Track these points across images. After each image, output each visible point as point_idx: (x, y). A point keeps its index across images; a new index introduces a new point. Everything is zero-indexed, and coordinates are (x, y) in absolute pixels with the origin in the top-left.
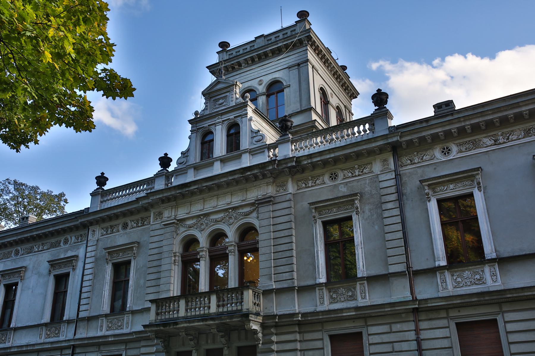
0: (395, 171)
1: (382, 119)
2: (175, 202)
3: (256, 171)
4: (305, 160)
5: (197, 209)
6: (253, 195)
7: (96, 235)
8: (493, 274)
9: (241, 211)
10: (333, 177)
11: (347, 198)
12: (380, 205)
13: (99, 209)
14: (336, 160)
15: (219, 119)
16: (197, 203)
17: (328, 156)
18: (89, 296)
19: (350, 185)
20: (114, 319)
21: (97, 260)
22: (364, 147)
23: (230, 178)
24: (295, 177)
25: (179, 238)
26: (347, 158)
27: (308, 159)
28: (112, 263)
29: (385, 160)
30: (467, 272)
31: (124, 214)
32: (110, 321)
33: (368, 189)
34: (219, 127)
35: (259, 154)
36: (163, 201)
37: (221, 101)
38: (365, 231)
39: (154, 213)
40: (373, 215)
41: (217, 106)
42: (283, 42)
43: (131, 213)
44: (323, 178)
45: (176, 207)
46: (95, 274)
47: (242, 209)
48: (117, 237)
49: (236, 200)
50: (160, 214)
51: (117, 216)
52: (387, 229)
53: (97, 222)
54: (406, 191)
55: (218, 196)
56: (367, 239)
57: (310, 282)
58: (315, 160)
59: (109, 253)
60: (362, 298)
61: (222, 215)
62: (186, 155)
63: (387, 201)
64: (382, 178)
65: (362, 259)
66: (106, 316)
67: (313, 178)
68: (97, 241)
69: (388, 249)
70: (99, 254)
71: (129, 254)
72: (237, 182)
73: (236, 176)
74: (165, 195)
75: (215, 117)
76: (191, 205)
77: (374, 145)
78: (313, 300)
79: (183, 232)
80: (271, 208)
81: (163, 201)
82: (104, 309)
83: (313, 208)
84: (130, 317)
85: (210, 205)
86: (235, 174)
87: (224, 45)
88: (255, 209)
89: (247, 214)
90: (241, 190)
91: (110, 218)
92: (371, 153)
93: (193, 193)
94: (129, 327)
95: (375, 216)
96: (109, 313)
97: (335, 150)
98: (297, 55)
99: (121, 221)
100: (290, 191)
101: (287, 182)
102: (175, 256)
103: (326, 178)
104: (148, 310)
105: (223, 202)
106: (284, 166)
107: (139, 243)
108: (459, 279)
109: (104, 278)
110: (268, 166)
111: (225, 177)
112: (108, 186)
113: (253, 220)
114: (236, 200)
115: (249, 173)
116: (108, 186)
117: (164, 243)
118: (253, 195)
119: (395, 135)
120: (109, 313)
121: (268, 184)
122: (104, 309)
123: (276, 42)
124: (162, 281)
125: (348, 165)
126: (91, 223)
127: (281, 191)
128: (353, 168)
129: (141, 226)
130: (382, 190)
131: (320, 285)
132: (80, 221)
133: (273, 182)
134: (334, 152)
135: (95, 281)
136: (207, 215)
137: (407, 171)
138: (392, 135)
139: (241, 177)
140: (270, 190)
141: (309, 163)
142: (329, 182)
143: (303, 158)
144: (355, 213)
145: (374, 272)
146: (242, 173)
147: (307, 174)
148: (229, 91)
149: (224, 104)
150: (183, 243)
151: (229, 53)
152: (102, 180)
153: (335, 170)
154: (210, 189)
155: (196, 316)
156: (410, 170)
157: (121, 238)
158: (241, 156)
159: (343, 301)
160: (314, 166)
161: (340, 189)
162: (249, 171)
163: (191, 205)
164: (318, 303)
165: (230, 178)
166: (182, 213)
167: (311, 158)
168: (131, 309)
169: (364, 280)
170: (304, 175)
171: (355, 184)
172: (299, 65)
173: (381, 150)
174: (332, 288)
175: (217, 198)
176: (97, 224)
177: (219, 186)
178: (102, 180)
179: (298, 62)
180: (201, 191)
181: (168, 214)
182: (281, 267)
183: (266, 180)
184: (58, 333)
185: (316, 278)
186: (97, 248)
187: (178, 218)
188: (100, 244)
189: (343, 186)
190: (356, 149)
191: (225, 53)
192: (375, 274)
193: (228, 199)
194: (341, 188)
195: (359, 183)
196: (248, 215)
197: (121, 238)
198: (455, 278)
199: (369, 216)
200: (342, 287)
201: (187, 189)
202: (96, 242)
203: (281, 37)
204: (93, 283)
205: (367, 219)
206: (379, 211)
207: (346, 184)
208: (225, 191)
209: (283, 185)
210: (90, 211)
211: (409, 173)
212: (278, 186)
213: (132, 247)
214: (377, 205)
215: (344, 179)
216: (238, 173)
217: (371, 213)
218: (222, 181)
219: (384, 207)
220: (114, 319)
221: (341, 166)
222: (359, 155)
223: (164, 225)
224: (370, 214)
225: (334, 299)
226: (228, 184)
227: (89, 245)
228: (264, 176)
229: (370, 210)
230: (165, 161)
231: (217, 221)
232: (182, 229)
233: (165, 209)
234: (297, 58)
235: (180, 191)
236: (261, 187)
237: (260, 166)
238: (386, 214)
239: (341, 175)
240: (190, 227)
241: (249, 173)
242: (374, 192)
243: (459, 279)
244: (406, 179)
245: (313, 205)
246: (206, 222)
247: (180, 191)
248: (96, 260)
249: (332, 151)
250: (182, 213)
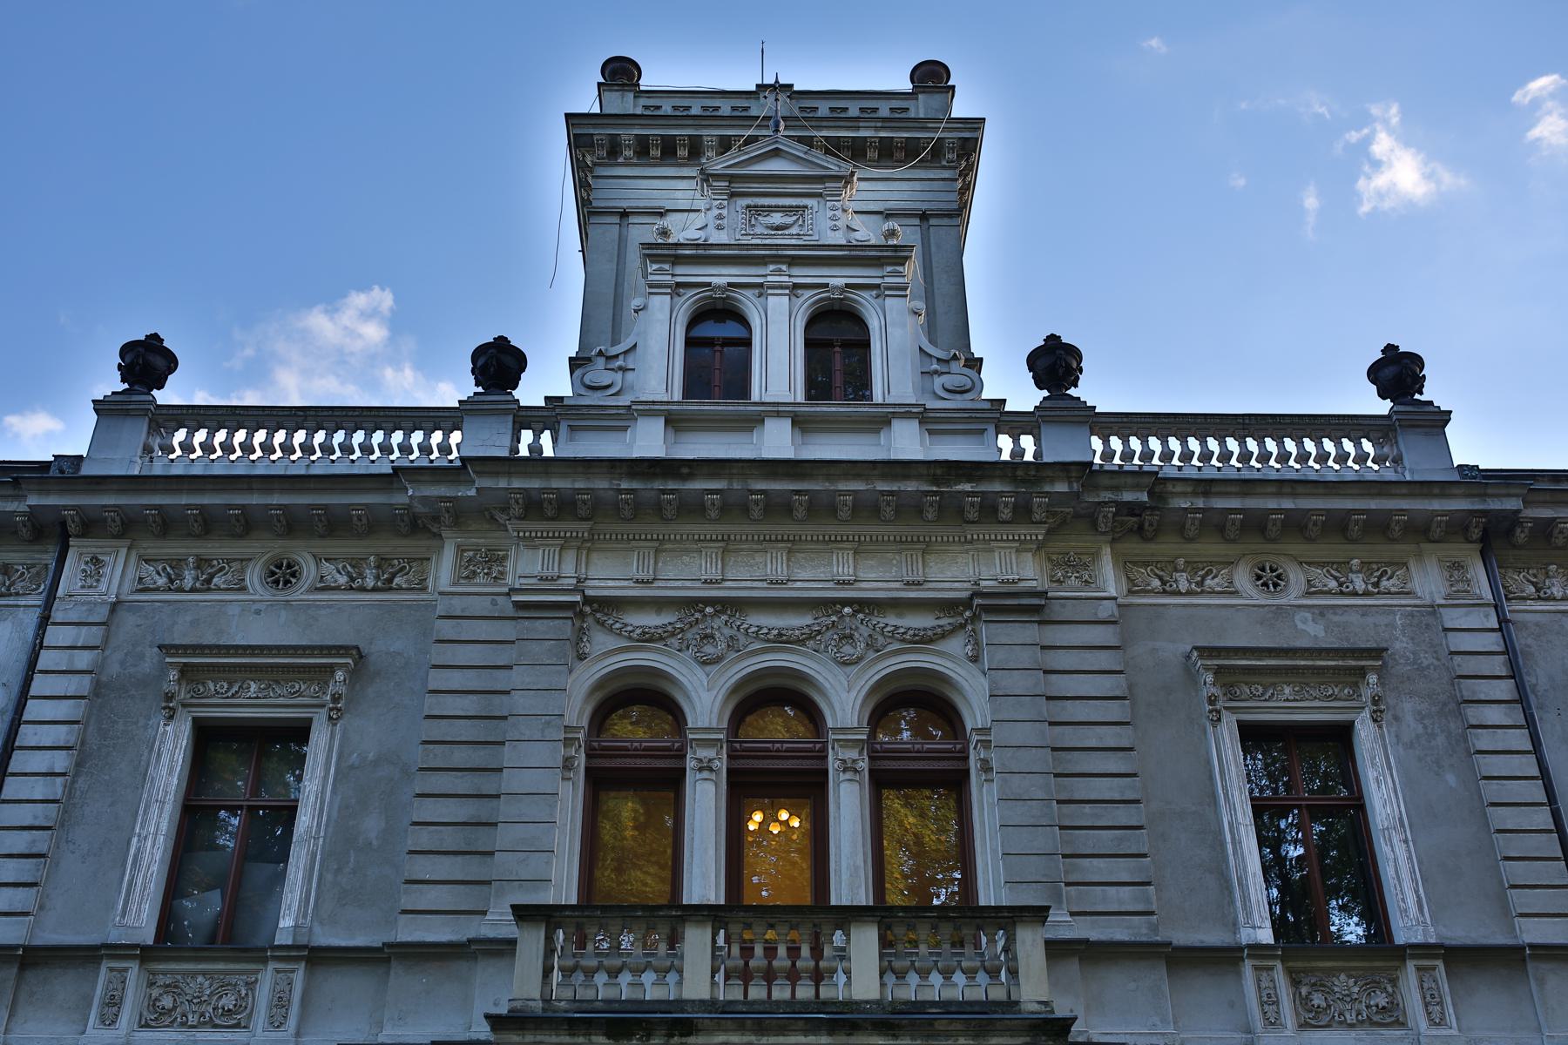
0: (1496, 607)
1: (1426, 434)
2: (586, 525)
3: (997, 487)
4: (1184, 494)
5: (688, 572)
6: (955, 572)
7: (101, 578)
8: (1269, 995)
9: (892, 620)
10: (1271, 580)
11: (1343, 658)
12: (1452, 706)
13: (136, 473)
14: (1296, 525)
15: (779, 272)
16: (687, 551)
17: (1272, 504)
18: (42, 848)
19: (1336, 618)
20: (194, 974)
21: (101, 692)
22: (1404, 504)
23: (882, 486)
24: (1118, 546)
25: (585, 677)
26: (1338, 526)
27: (1195, 494)
28: (194, 719)
29: (1457, 566)
30: (1343, 977)
31: (293, 525)
32: (161, 980)
33: (1401, 645)
34: (778, 304)
35: (960, 438)
36: (533, 507)
37: (777, 219)
38: (1409, 786)
39: (461, 550)
40: (1433, 736)
41: (759, 230)
42: (876, 129)
43: (334, 525)
44: (1231, 574)
45: (587, 546)
46: (83, 756)
47: (900, 615)
48: (234, 610)
49: (877, 576)
50: (494, 559)
51: (247, 525)
52: (1492, 791)
53: (128, 527)
54: (1534, 681)
55: (793, 546)
56: (1420, 817)
57: (1213, 937)
58: (1220, 503)
59: (186, 671)
60: (1433, 1023)
61: (808, 620)
62: (620, 363)
63: (1483, 697)
64: (1453, 618)
65: (1414, 880)
66: (144, 954)
67: (1192, 566)
68: (115, 607)
69: (1507, 859)
70: (114, 669)
71: (299, 694)
72: (909, 509)
73: (911, 486)
74: (556, 483)
75: (762, 261)
76: (657, 551)
77: (1436, 505)
78: (1232, 1005)
79: (608, 655)
80: (1031, 633)
81: (533, 507)
82: (129, 920)
83: (1207, 668)
84: (299, 977)
85: (750, 573)
86: (906, 477)
87: (620, 72)
88: (963, 626)
89: (923, 640)
90: (902, 543)
91: (208, 524)
92: (1421, 531)
93: (692, 508)
94: (292, 1023)
95: (1441, 740)
96: (150, 942)
97: (1300, 489)
98: (917, 186)
99: (261, 551)
100: (1113, 592)
101: (1096, 556)
102: (567, 742)
103: (1243, 578)
104: (504, 949)
105: (817, 573)
106: (1106, 496)
107: (359, 655)
108: (1318, 1000)
109: (141, 775)
110: (1052, 480)
111: (857, 477)
112: (168, 395)
113: (949, 661)
114: (877, 576)
115: (968, 487)
116: (168, 395)
117: (517, 678)
118: (955, 572)
119: (1513, 491)
120: (150, 942)
121: (1022, 546)
122: (129, 920)
123: (854, 122)
124: (504, 837)
125: (1338, 550)
126: (91, 525)
127: (1073, 582)
128: (1343, 565)
129: (375, 590)
130: (1457, 659)
131: (1257, 950)
132: (33, 500)
133: (1040, 546)
134: (1294, 495)
135: (82, 783)
136: (732, 606)
137: (1528, 617)
138: (1503, 491)
139: (927, 493)
140: (1028, 571)
141: (1198, 510)
142: (1252, 591)
143: (1179, 488)
144: (1366, 714)
145: (1472, 928)
146: (935, 480)
147: (1166, 547)
148: (820, 195)
149: (794, 230)
150: (599, 696)
151: (643, 101)
152: (147, 362)
153: (1272, 558)
154: (778, 508)
155: (792, 1004)
156: (1538, 617)
157: (251, 616)
158: (889, 423)
159: (1352, 1026)
160: (1216, 525)
161: (1300, 626)
162: (970, 479)
163: (657, 551)
164: (1259, 1024)
165: (882, 486)
166: (610, 574)
167: (1206, 494)
168: (303, 941)
169: (1436, 957)
170: (1151, 548)
171: (1354, 618)
172: (924, 216)
173: (1457, 528)
174: (1306, 971)
175: (790, 551)
176: (119, 536)
177: (820, 508)
178: (147, 362)
179: (924, 207)
180: (736, 508)
181: (527, 565)
182: (1095, 861)
183: (1023, 531)
184: (238, 1008)
185: (1235, 924)
186: (106, 639)
187: (589, 592)
188: (128, 623)
189: (1309, 616)
190: (1373, 504)
191: (631, 95)
192: (1469, 942)
193: (842, 566)
194: (1305, 622)
195: (1370, 620)
196: (931, 641)
197: (251, 616)
198: (1304, 991)
199: (1418, 737)
200: (204, 973)
201: (671, 485)
202: (105, 610)
203: (884, 111)
204: (70, 789)
205: (1410, 746)
206: (1455, 726)
207: (1322, 611)
208: (833, 530)
209: (1079, 565)
210: (86, 470)
211: (1537, 624)
212: (1056, 564)
213: (331, 669)
214: (1445, 704)
215: (1308, 594)
216: (919, 477)
217: (1425, 727)
218: (842, 486)
219: (1475, 714)
220: (194, 974)
221: (1298, 548)
222: (1379, 527)
223: (519, 605)
224: (1420, 730)
225: (1318, 1011)
226: (866, 509)
227: (57, 615)
228: (1023, 513)
229: (1420, 717)
230: (499, 365)
231: (782, 640)
232: (600, 641)
233: (531, 542)
234: (929, 196)
235: (635, 485)
236: (992, 551)
237: (1020, 473)
238: (1484, 740)
239: (1296, 578)
240: (648, 638)
241: (968, 487)
242: (1427, 659)
243: (1318, 1000)
244: (1529, 641)
245: (1210, 657)
246: (727, 631)
247: (635, 485)
248: (98, 689)
249: (1287, 489)
250: (610, 574)
